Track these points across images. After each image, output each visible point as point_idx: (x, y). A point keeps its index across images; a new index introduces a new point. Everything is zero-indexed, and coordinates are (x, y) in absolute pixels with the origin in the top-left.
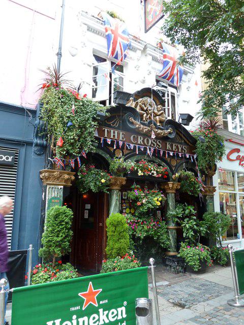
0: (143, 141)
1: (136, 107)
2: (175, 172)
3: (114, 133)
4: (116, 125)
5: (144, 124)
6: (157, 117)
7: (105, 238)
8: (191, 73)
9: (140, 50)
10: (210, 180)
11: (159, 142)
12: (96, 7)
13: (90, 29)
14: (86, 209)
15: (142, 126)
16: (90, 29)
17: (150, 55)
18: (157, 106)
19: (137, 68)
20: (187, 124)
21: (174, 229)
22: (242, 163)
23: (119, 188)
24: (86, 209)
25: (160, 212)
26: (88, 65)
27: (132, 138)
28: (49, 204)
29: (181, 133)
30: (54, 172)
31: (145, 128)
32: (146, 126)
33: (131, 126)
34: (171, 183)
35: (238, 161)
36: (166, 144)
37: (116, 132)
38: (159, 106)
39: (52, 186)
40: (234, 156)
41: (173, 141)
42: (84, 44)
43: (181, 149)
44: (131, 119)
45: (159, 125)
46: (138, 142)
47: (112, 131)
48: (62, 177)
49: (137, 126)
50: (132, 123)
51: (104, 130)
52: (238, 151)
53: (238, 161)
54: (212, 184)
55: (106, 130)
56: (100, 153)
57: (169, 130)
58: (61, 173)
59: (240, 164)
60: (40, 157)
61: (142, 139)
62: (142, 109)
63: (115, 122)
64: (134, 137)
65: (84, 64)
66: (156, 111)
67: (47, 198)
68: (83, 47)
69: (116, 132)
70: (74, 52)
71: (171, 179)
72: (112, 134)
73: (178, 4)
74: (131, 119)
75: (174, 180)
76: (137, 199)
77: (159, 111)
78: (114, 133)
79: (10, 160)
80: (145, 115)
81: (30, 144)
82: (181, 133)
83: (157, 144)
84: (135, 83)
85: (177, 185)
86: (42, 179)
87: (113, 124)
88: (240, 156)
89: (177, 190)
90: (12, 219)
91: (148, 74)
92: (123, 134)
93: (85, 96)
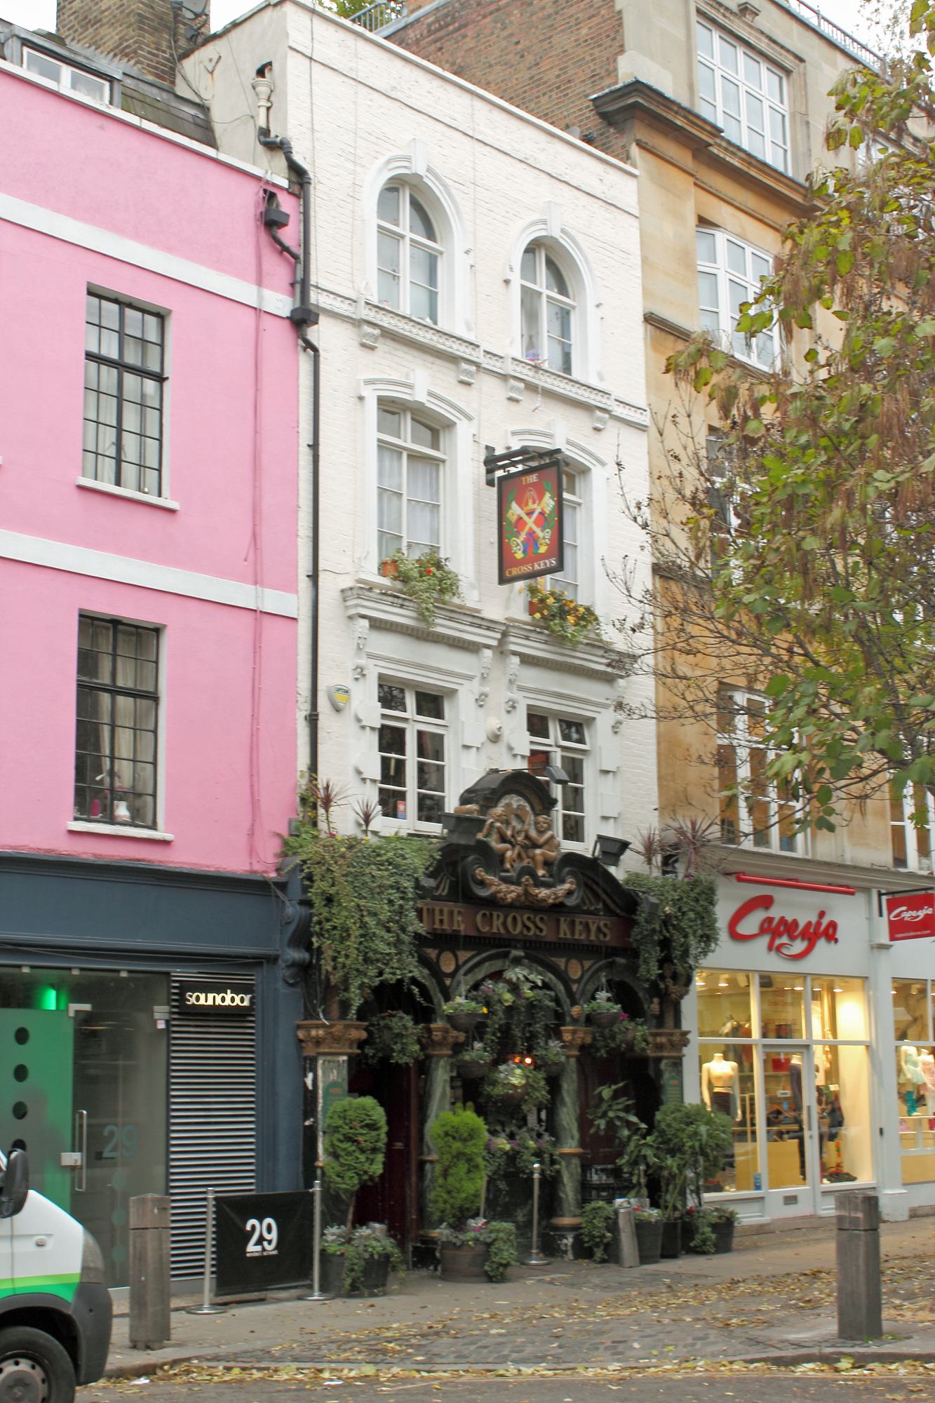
0: (504, 924)
2: (577, 996)
5: (506, 880)
6: (538, 851)
7: (414, 1179)
8: (622, 677)
9: (488, 647)
10: (672, 1013)
13: (377, 625)
16: (377, 625)
17: (515, 653)
20: (616, 863)
21: (574, 1155)
22: (778, 942)
23: (450, 1052)
27: (479, 918)
28: (324, 1098)
29: (597, 884)
31: (513, 891)
32: (513, 883)
34: (568, 1031)
35: (766, 939)
36: (558, 921)
40: (749, 925)
41: (576, 910)
43: (599, 928)
44: (480, 873)
45: (543, 876)
50: (482, 883)
52: (766, 902)
53: (766, 939)
54: (678, 1023)
57: (567, 886)
59: (770, 948)
60: (293, 989)
64: (484, 915)
66: (533, 833)
67: (321, 1085)
68: (357, 679)
71: (568, 1019)
74: (480, 873)
75: (575, 1021)
79: (246, 1003)
80: (509, 854)
81: (273, 960)
82: (597, 884)
83: (537, 927)
85: (583, 1035)
86: (301, 1041)
88: (770, 920)
89: (583, 1048)
90: (173, 1121)
91: (508, 712)
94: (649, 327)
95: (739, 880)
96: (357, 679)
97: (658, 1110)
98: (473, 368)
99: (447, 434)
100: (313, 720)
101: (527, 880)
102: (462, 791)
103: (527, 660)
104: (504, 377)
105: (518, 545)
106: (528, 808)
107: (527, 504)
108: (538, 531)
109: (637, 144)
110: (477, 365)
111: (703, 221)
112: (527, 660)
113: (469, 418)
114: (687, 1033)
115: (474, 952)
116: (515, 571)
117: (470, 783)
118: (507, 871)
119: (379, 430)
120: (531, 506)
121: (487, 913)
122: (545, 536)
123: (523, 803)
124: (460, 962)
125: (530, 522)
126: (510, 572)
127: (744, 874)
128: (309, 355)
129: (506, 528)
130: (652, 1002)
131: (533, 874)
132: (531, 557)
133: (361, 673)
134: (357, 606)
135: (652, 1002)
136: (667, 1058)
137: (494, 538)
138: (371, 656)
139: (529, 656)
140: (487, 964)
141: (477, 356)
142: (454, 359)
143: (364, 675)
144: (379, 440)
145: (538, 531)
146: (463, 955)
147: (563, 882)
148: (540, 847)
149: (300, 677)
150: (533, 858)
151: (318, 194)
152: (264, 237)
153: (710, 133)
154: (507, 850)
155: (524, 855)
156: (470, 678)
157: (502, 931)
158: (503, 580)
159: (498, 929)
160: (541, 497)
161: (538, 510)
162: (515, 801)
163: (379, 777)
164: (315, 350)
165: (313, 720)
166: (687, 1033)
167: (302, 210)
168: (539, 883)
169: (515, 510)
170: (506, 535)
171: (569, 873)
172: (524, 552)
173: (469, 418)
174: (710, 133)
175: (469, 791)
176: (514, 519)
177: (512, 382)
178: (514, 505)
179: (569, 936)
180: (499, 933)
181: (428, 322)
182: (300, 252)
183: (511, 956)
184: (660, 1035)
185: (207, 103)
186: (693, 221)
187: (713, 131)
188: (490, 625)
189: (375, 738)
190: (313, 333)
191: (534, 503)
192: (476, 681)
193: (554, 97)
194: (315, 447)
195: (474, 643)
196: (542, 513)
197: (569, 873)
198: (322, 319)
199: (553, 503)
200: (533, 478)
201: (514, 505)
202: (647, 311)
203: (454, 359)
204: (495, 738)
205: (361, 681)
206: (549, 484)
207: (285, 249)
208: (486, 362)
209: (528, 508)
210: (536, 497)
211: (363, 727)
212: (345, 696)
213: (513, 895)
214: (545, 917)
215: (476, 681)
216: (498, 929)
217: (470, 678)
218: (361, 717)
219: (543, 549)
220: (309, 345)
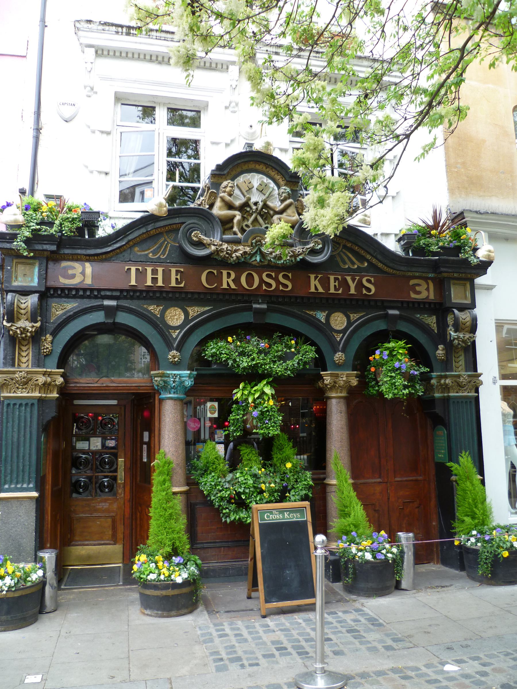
0: (237, 281)
1: (211, 206)
9: (233, 63)
11: (285, 277)
15: (225, 246)
19: (231, 109)
25: (216, 404)
26: (102, 132)
30: (14, 373)
31: (236, 251)
42: (92, 89)
44: (197, 235)
47: (149, 270)
51: (129, 269)
61: (233, 275)
63: (160, 247)
65: (93, 132)
69: (160, 270)
70: (68, 112)
72: (149, 276)
73: (39, 227)
93: (265, 115)
123: (266, 180)
146: (194, 311)
157: (233, 286)
159: (228, 284)
166: (480, 375)
184: (446, 377)
216: (228, 284)
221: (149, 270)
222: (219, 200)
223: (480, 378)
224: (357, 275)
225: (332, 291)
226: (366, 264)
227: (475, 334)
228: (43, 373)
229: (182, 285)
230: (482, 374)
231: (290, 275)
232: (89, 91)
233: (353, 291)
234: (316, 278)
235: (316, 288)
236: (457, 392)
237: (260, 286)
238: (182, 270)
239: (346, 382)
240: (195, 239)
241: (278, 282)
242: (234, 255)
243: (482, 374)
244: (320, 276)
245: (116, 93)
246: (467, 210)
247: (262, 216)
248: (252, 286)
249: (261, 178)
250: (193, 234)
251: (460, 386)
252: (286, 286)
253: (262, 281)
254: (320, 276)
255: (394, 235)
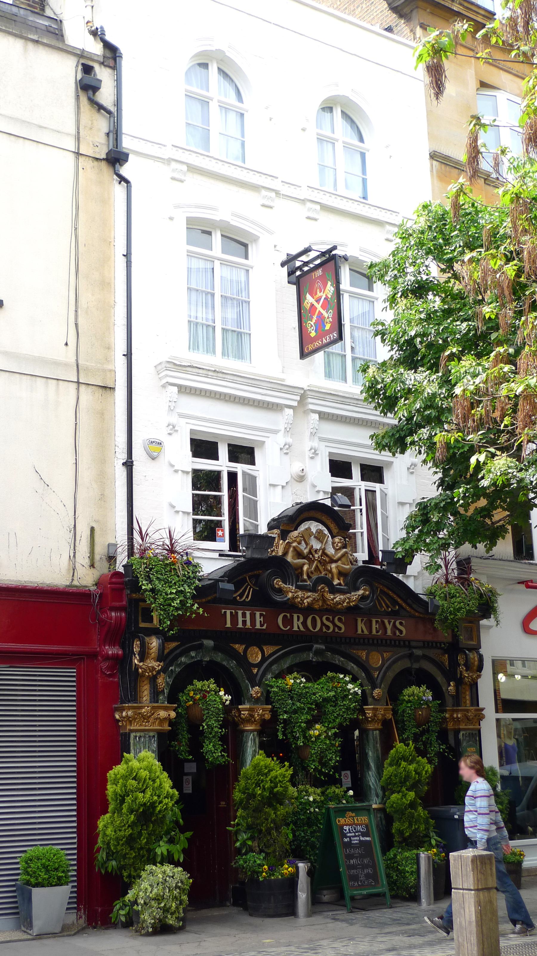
0: (304, 624)
1: (285, 553)
3: (244, 615)
4: (247, 597)
6: (333, 565)
9: (290, 407)
11: (340, 620)
12: (165, 146)
13: (183, 390)
14: (188, 774)
15: (300, 593)
16: (183, 390)
18: (333, 537)
24: (188, 774)
25: (348, 772)
31: (308, 597)
33: (278, 598)
36: (356, 620)
37: (248, 613)
38: (337, 540)
39: (138, 734)
42: (174, 427)
44: (278, 583)
45: (340, 584)
46: (292, 627)
47: (240, 613)
48: (155, 715)
49: (290, 595)
50: (280, 591)
51: (225, 612)
55: (228, 612)
56: (219, 660)
57: (361, 592)
58: (153, 708)
62: (299, 554)
64: (285, 617)
68: (170, 434)
69: (248, 613)
74: (278, 583)
76: (478, 461)
77: (337, 550)
78: (244, 615)
80: (305, 568)
84: (283, 487)
87: (241, 596)
92: (261, 615)
94: (435, 163)
95: (528, 587)
96: (170, 434)
97: (169, 777)
98: (273, 195)
99: (254, 245)
100: (129, 465)
101: (323, 588)
102: (269, 519)
103: (324, 416)
104: (303, 201)
105: (312, 326)
106: (326, 532)
107: (316, 294)
108: (324, 312)
109: (421, 27)
110: (277, 193)
111: (483, 85)
112: (324, 416)
113: (270, 232)
114: (483, 709)
115: (277, 648)
116: (311, 347)
117: (275, 514)
118: (305, 581)
119: (188, 243)
120: (319, 294)
121: (288, 615)
122: (328, 315)
123: (321, 527)
124: (266, 654)
125: (319, 307)
126: (308, 349)
127: (532, 581)
128: (123, 186)
129: (303, 314)
130: (450, 685)
131: (328, 582)
132: (321, 334)
133: (173, 429)
134: (167, 376)
135: (450, 685)
136: (464, 729)
137: (296, 324)
138: (182, 416)
139: (324, 413)
140: (399, 663)
141: (275, 185)
142: (255, 188)
143: (177, 431)
144: (188, 251)
145: (324, 312)
146: (269, 650)
147: (358, 589)
148: (336, 561)
149: (117, 433)
150: (330, 571)
151: (126, 64)
152: (84, 99)
153: (484, 16)
154: (304, 564)
155: (321, 568)
156: (276, 432)
157: (302, 629)
158: (303, 355)
159: (298, 627)
160: (325, 285)
161: (324, 297)
162: (314, 526)
163: (190, 510)
164: (127, 182)
165: (129, 465)
166: (483, 709)
167: (116, 79)
168: (334, 590)
169: (309, 299)
170: (303, 320)
171: (362, 582)
172: (316, 331)
173: (270, 232)
174: (484, 16)
175: (273, 520)
176: (308, 306)
177: (309, 205)
178: (308, 296)
179: (366, 632)
180: (300, 630)
181: (240, 164)
182: (113, 109)
183: (314, 649)
184: (457, 711)
185: (61, 17)
186: (473, 84)
187: (487, 14)
188: (290, 389)
189: (188, 480)
190: (125, 170)
191: (320, 292)
192: (281, 434)
193: (364, 7)
194: (128, 256)
195: (277, 405)
196: (326, 298)
197: (362, 582)
198: (131, 157)
199: (333, 289)
200: (319, 272)
201: (308, 296)
202: (431, 151)
203: (255, 188)
204: (301, 478)
205: (175, 435)
206: (330, 275)
207: (100, 107)
208: (285, 190)
209: (317, 296)
210: (322, 287)
211: (176, 471)
212: (158, 447)
213: (309, 600)
214: (404, 622)
215: (281, 434)
216: (298, 627)
217: (276, 432)
218: (173, 464)
219: (328, 327)
220: (122, 179)
221: (240, 613)
222: (291, 549)
223: (483, 712)
224: (393, 619)
225: (374, 632)
226: (397, 607)
227: (480, 672)
228: (174, 708)
229: (264, 627)
230: (484, 709)
231: (343, 618)
232: (171, 430)
233: (389, 632)
234: (362, 620)
235: (362, 631)
236: (466, 725)
237: (321, 629)
238: (264, 613)
239: (383, 715)
240: (277, 586)
241: (335, 625)
242: (305, 601)
243: (484, 709)
244: (365, 619)
245: (191, 429)
246: (474, 557)
247: (321, 563)
248: (284, 615)
249: (317, 525)
250: (275, 582)
251: (468, 719)
252: (340, 629)
253: (323, 624)
254: (365, 619)
255: (412, 578)
